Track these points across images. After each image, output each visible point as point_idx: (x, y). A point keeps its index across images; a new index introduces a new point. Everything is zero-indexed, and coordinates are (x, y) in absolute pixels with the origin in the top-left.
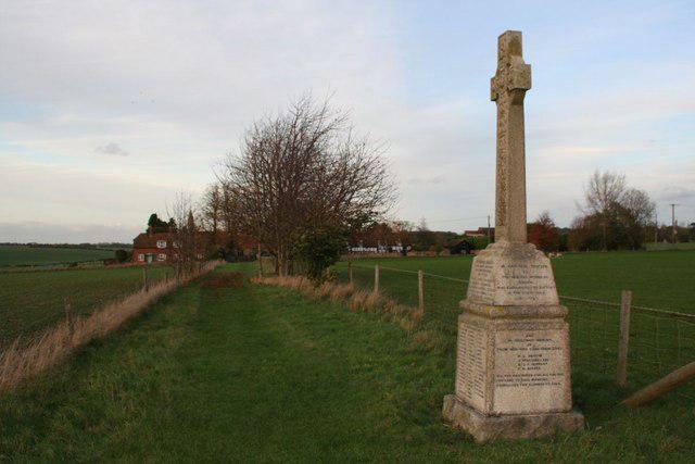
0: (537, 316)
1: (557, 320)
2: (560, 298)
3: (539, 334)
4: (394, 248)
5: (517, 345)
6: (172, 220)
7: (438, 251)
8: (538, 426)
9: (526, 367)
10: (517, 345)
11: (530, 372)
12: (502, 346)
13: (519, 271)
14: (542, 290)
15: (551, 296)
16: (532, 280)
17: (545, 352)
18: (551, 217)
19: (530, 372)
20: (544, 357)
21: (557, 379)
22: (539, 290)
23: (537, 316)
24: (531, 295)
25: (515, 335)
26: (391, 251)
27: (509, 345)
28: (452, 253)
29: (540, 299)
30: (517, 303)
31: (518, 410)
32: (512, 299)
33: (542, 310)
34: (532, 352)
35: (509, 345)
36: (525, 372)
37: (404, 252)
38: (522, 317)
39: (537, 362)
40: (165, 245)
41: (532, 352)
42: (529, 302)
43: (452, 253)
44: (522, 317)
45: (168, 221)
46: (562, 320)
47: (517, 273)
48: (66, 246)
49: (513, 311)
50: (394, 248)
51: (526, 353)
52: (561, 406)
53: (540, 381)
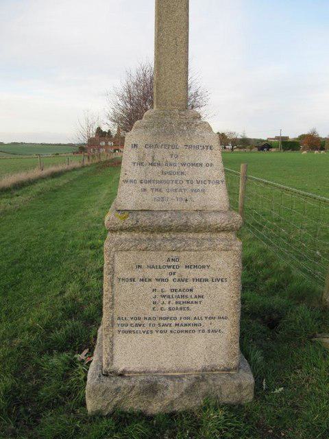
0: (185, 228)
1: (223, 235)
2: (230, 201)
3: (186, 257)
4: (227, 147)
5: (150, 273)
6: (109, 131)
7: (251, 149)
8: (176, 395)
9: (166, 306)
10: (150, 273)
11: (172, 314)
12: (128, 275)
13: (161, 154)
14: (200, 187)
15: (217, 196)
16: (185, 169)
17: (198, 284)
18: (317, 130)
19: (172, 314)
20: (197, 291)
21: (217, 324)
22: (195, 186)
23: (185, 228)
24: (179, 194)
25: (147, 258)
26: (225, 148)
27: (138, 274)
28: (259, 150)
29: (197, 201)
30: (156, 206)
31: (153, 367)
32: (148, 200)
33: (195, 220)
34: (177, 285)
35: (138, 274)
36: (164, 314)
37: (232, 149)
38: (160, 229)
39: (184, 299)
40: (104, 143)
41: (177, 285)
42: (177, 205)
43: (259, 150)
44: (160, 229)
45: (107, 131)
46: (232, 236)
47: (158, 158)
48: (60, 145)
49: (144, 220)
50: (227, 147)
51: (166, 287)
52: (221, 361)
53: (189, 327)
